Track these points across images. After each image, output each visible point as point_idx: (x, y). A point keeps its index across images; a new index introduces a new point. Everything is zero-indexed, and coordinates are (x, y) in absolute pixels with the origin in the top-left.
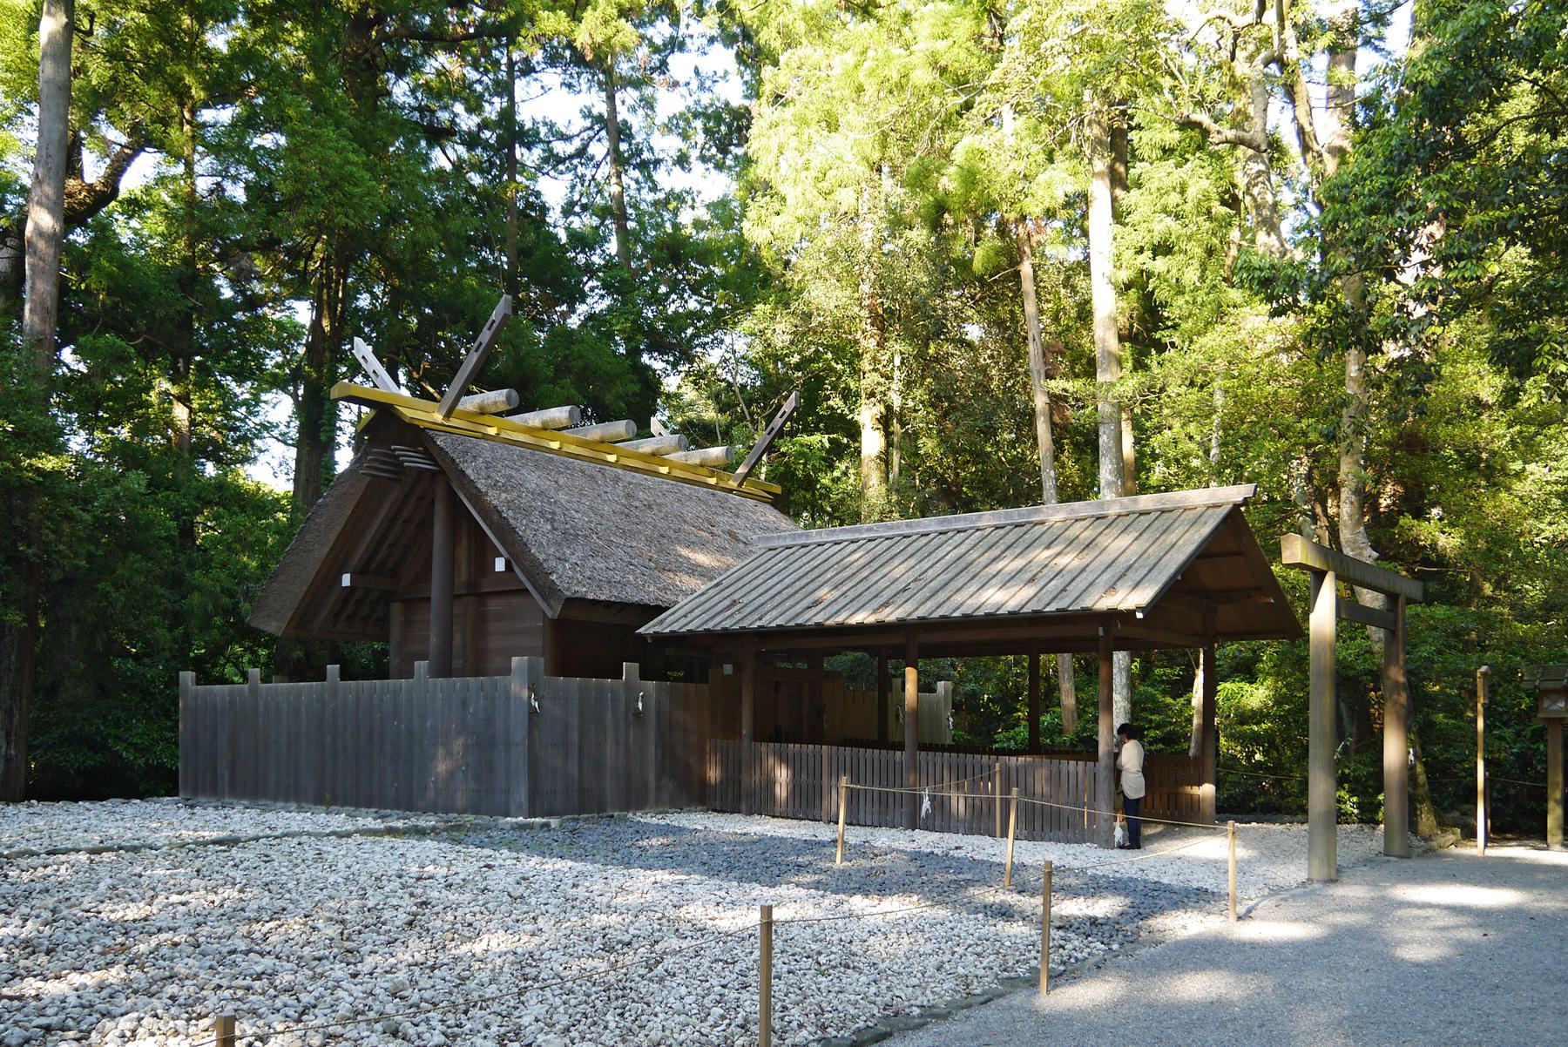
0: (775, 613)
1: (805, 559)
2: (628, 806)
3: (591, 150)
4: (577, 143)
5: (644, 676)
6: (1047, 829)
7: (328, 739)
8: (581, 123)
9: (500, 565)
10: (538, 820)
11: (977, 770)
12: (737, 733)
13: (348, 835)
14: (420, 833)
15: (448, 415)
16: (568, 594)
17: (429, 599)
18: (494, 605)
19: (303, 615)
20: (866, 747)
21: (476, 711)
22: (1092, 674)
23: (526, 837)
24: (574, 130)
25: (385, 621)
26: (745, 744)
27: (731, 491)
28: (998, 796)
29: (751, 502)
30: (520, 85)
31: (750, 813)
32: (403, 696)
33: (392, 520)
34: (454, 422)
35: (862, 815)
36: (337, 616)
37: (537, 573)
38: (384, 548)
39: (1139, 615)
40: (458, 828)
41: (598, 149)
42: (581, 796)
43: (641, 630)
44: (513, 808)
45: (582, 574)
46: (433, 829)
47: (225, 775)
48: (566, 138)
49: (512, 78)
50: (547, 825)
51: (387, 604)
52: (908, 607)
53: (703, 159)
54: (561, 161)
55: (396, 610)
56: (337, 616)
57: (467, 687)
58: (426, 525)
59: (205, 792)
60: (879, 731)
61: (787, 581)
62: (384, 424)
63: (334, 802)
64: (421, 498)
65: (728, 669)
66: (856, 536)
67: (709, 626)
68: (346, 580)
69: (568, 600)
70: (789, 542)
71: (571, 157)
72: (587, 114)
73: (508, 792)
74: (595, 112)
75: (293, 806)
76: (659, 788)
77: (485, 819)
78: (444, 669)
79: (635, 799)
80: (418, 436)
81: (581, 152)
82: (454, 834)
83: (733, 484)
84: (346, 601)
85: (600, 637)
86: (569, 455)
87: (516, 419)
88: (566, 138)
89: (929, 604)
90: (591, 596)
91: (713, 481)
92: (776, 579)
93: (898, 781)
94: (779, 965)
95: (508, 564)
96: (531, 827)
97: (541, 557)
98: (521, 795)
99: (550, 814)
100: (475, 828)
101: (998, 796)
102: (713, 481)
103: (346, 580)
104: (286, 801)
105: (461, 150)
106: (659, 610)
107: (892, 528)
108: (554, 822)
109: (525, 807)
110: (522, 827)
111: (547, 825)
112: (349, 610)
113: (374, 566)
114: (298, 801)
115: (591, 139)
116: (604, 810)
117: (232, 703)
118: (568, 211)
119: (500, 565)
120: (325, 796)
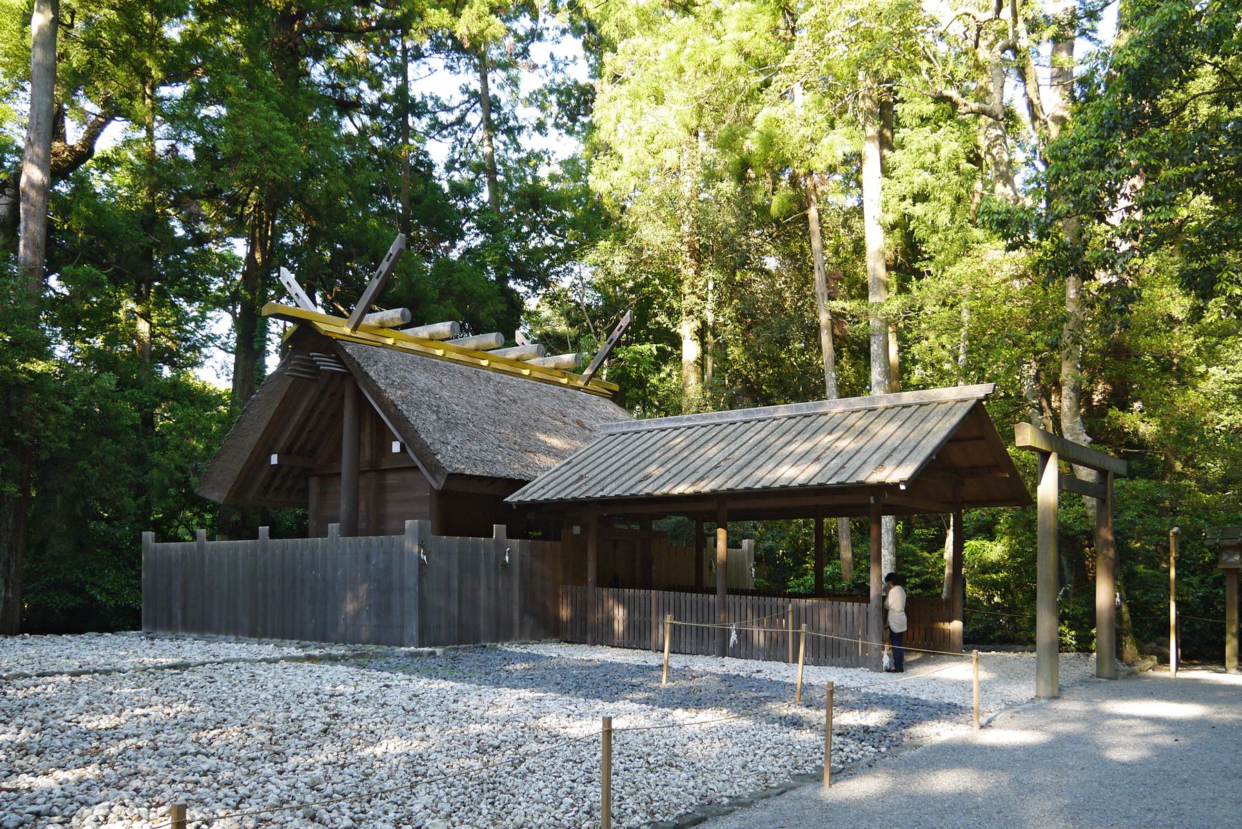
0: (613, 485)
1: (637, 443)
2: (497, 638)
3: (468, 119)
4: (457, 113)
5: (510, 535)
6: (829, 656)
7: (260, 585)
8: (460, 97)
9: (396, 447)
10: (426, 649)
11: (774, 610)
12: (584, 580)
13: (276, 661)
14: (333, 659)
15: (355, 329)
16: (450, 470)
17: (340, 474)
18: (392, 479)
19: (240, 487)
20: (686, 591)
21: (377, 563)
22: (865, 534)
23: (417, 663)
24: (455, 103)
25: (305, 491)
26: (590, 589)
27: (579, 389)
28: (790, 630)
29: (595, 398)
30: (412, 68)
31: (594, 644)
32: (319, 551)
33: (310, 412)
34: (359, 334)
35: (683, 645)
36: (267, 488)
37: (426, 453)
38: (305, 434)
39: (903, 487)
40: (362, 655)
41: (474, 118)
42: (460, 630)
43: (508, 499)
44: (406, 640)
45: (461, 454)
46: (343, 656)
47: (179, 613)
48: (448, 109)
49: (405, 62)
50: (433, 653)
51: (307, 479)
52: (719, 481)
53: (557, 126)
54: (445, 127)
55: (314, 483)
56: (267, 488)
57: (370, 544)
58: (337, 416)
59: (162, 627)
60: (696, 579)
61: (623, 460)
62: (304, 336)
63: (265, 635)
64: (333, 394)
65: (577, 530)
66: (678, 424)
67: (562, 495)
68: (274, 459)
69: (450, 475)
70: (625, 429)
71: (452, 124)
72: (465, 90)
73: (402, 627)
74: (471, 89)
75: (232, 638)
76: (522, 624)
77: (384, 649)
78: (352, 530)
79: (503, 633)
80: (331, 345)
81: (460, 121)
82: (360, 660)
83: (581, 383)
84: (274, 476)
85: (475, 504)
86: (451, 360)
87: (409, 332)
88: (448, 109)
89: (736, 478)
90: (468, 472)
91: (564, 381)
92: (614, 459)
93: (711, 618)
94: (617, 764)
95: (402, 446)
96: (420, 654)
97: (429, 441)
98: (413, 629)
99: (436, 645)
100: (376, 656)
101: (790, 630)
102: (564, 381)
103: (274, 459)
104: (227, 634)
105: (366, 118)
106: (522, 483)
107: (706, 418)
108: (439, 651)
109: (416, 639)
110: (414, 655)
111: (433, 653)
112: (277, 483)
113: (296, 448)
114: (236, 634)
115: (468, 110)
116: (478, 642)
117: (184, 557)
118: (450, 167)
119: (396, 447)
120: (258, 630)
